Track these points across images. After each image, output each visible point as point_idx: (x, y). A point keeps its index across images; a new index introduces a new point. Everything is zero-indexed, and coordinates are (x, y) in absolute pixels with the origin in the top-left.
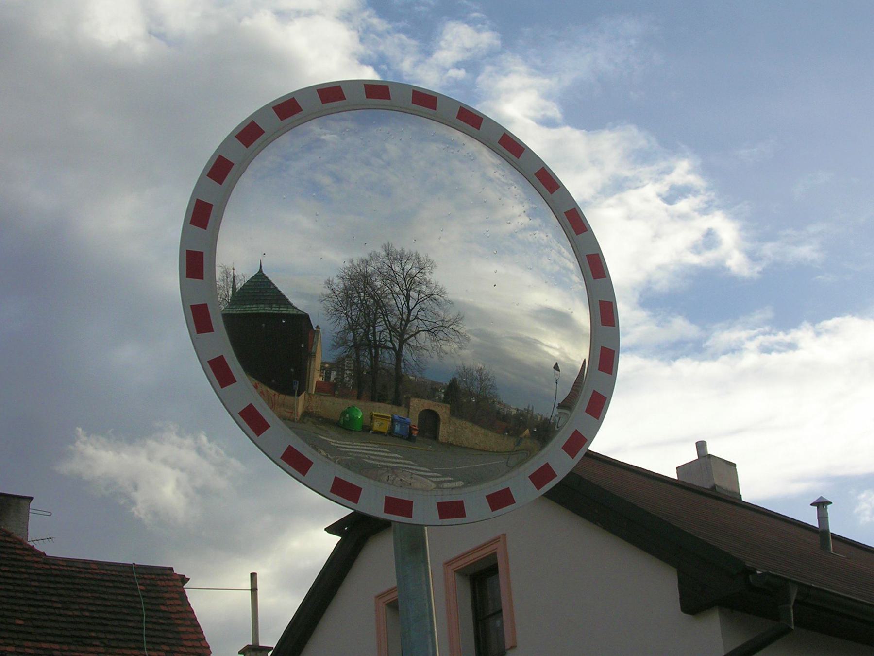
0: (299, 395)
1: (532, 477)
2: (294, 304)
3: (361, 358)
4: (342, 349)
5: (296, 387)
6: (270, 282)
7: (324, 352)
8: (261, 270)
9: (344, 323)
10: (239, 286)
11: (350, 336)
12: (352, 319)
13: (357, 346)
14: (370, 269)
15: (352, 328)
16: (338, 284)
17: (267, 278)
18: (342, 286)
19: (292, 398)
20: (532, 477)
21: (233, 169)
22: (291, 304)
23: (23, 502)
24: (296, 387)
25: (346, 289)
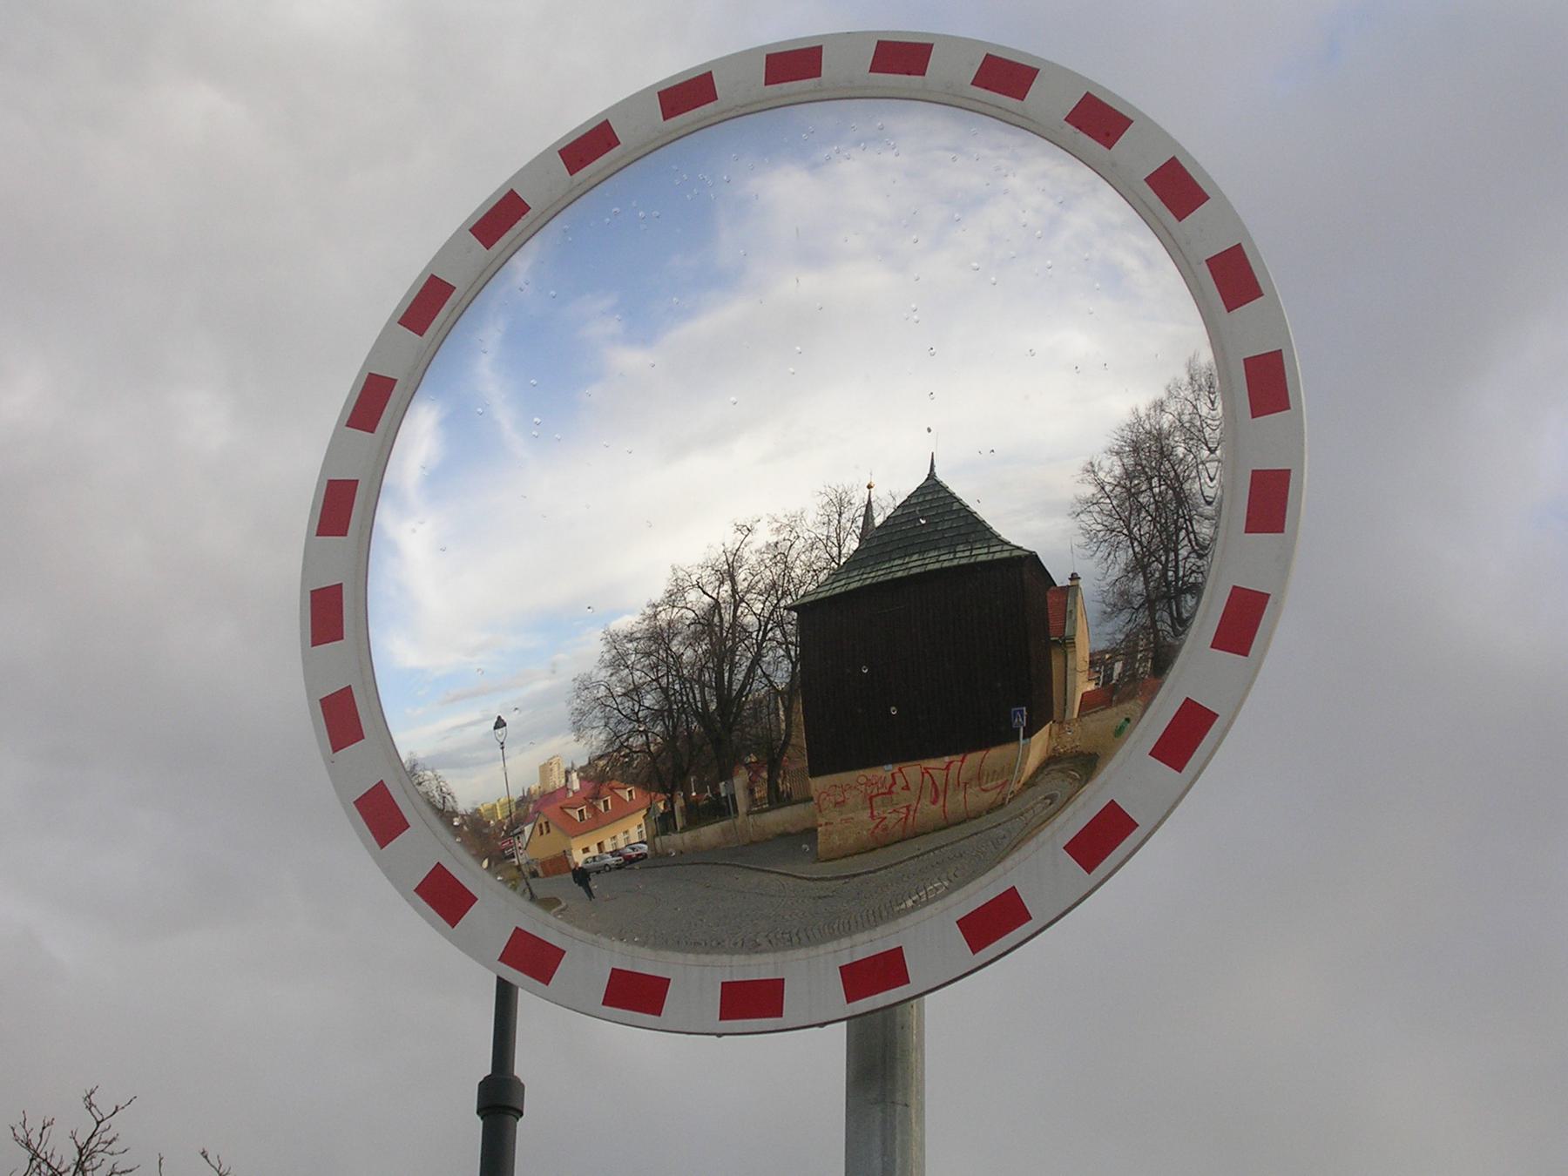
0: (1029, 733)
1: (963, 923)
2: (1004, 536)
3: (1159, 624)
4: (1125, 616)
5: (1021, 721)
6: (952, 495)
7: (1090, 632)
8: (931, 475)
9: (1124, 557)
10: (878, 521)
11: (1138, 585)
12: (1140, 543)
13: (1150, 603)
14: (1166, 421)
15: (1139, 566)
16: (1111, 469)
17: (945, 489)
18: (1118, 471)
19: (1011, 747)
20: (963, 923)
21: (1168, 216)
22: (997, 537)
23: (898, 1009)
24: (1021, 721)
25: (1129, 475)
